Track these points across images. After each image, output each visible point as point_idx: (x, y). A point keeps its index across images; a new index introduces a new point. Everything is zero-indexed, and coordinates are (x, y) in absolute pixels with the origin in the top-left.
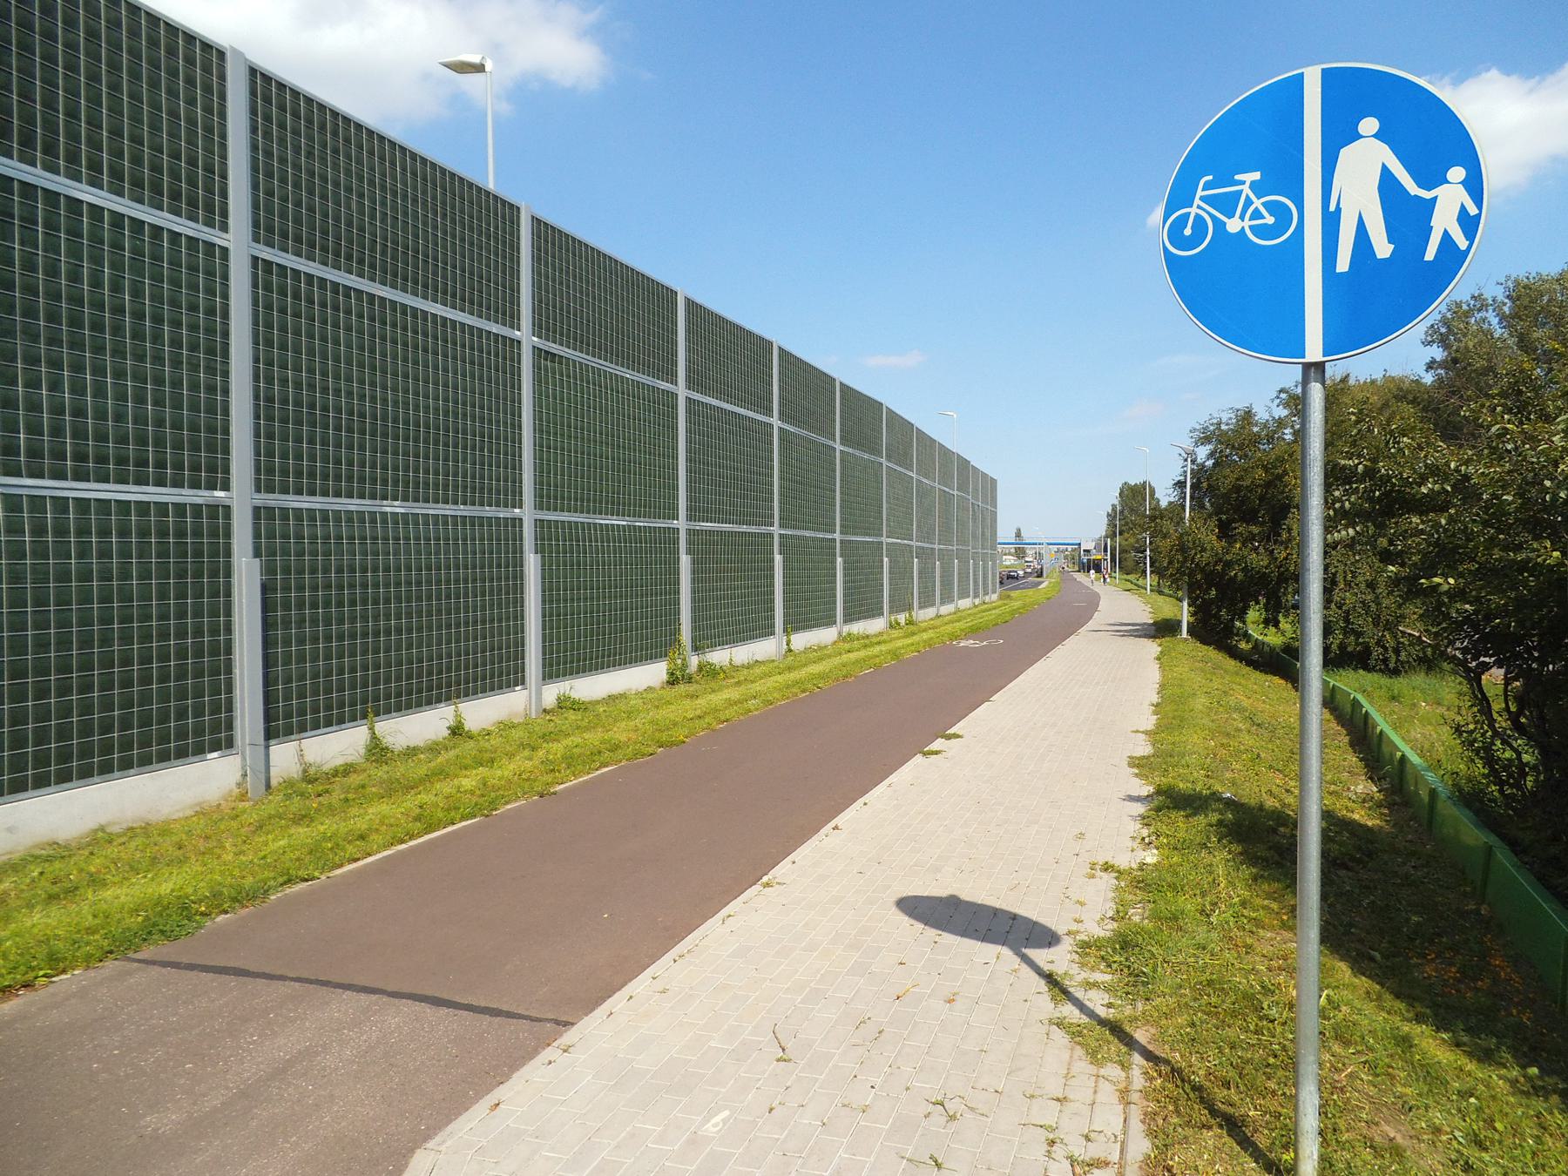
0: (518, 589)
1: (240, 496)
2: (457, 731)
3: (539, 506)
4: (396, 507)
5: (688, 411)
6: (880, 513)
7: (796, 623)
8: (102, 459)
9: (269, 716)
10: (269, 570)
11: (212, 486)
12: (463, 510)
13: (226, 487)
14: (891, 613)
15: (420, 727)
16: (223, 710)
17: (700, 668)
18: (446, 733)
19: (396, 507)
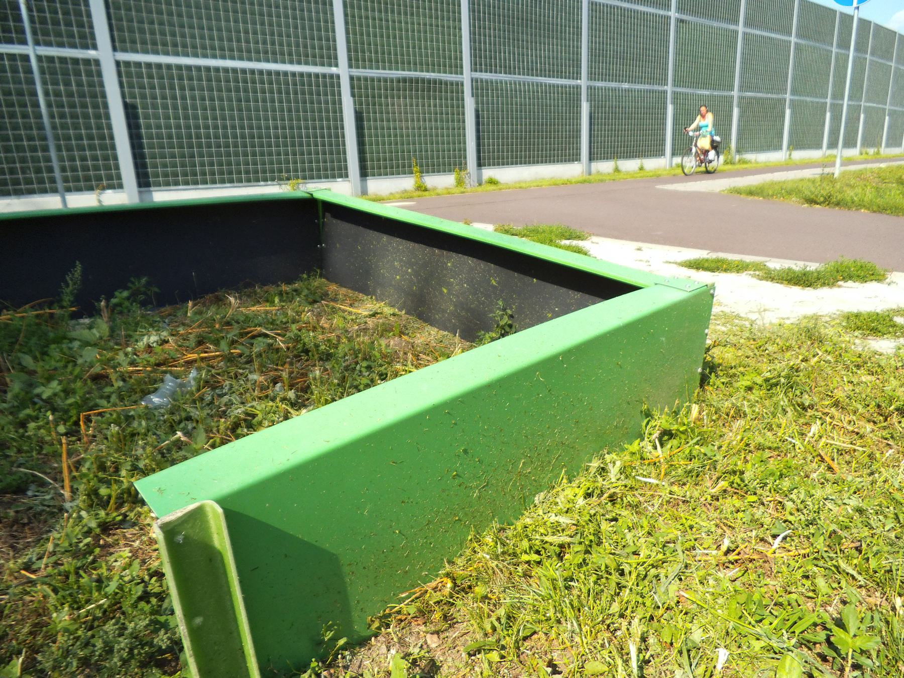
0: (664, 119)
1: (735, 93)
2: (641, 169)
3: (674, 85)
4: (626, 86)
5: (744, 39)
6: (862, 88)
7: (797, 144)
8: (249, 51)
9: (479, 158)
10: (477, 103)
11: (330, 65)
12: (647, 87)
13: (337, 65)
14: (673, 154)
15: (630, 165)
16: (856, 143)
17: (739, 161)
18: (637, 169)
19: (626, 86)
